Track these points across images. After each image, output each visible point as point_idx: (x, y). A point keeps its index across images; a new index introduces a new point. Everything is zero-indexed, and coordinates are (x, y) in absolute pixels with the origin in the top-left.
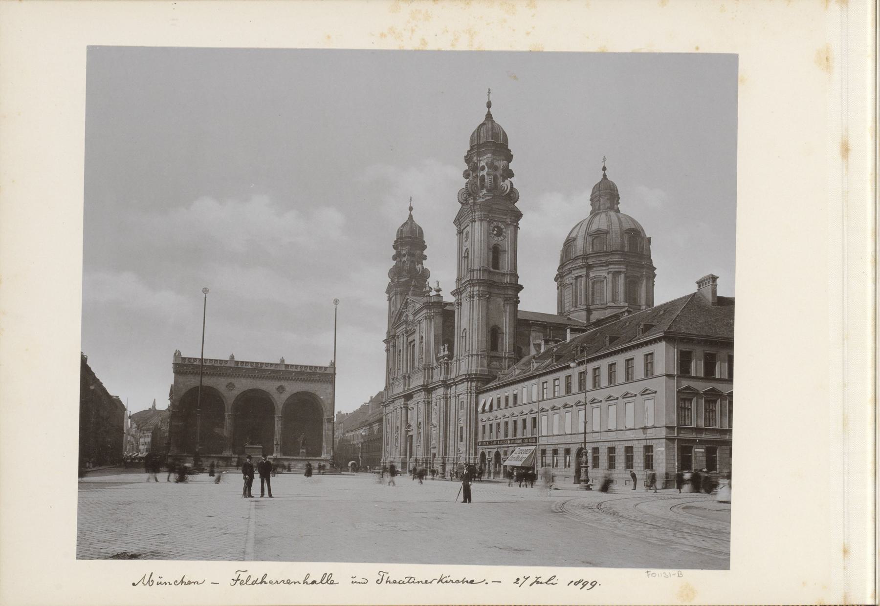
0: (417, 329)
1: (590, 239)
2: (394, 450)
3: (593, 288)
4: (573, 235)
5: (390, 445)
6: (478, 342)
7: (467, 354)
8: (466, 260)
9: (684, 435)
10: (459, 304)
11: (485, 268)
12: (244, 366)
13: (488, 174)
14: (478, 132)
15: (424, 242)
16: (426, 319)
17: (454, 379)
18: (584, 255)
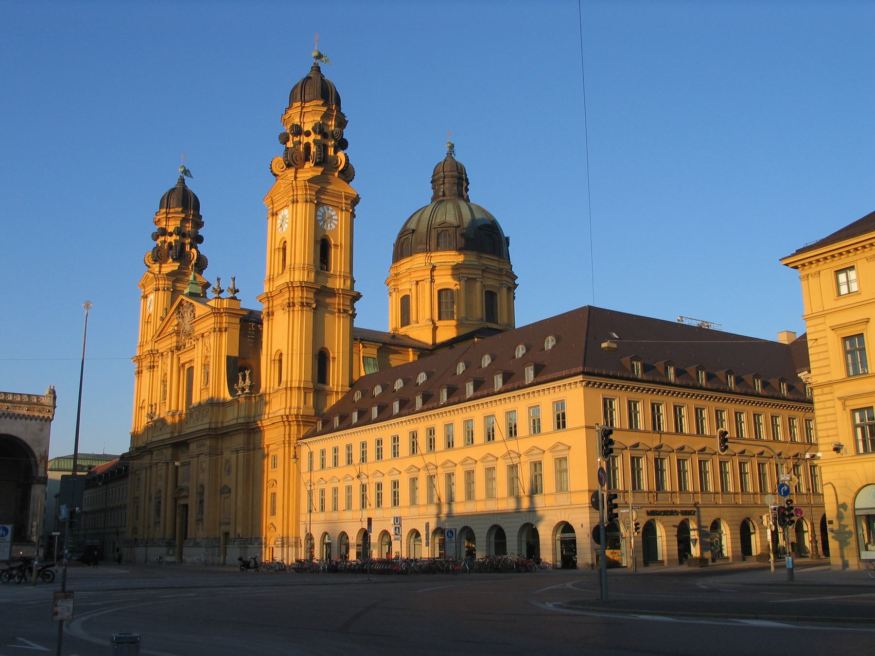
4: (412, 226)
10: (270, 314)
13: (315, 141)
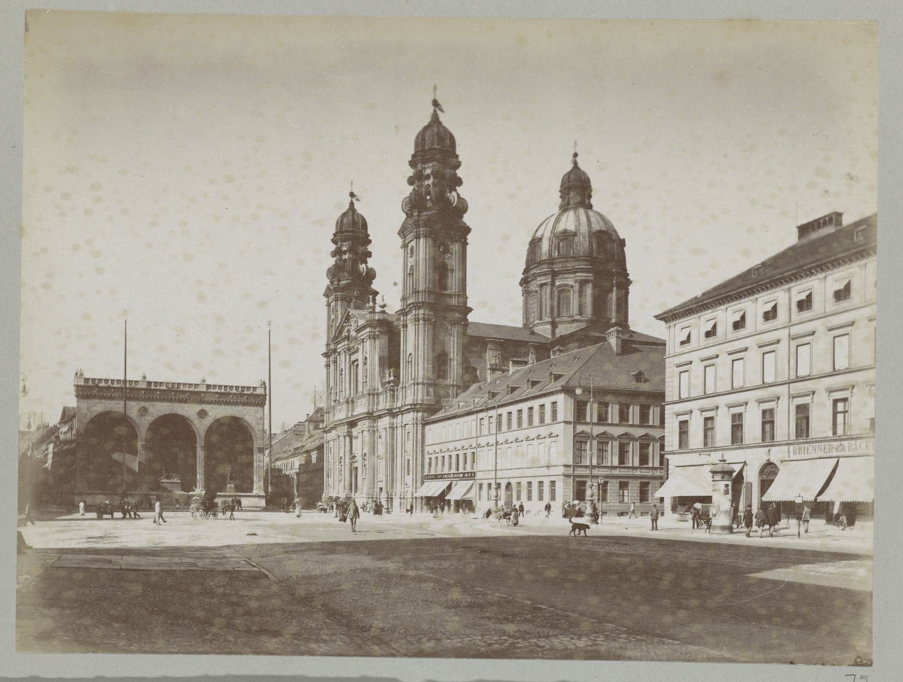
0: (361, 347)
1: (555, 242)
2: (337, 483)
3: (559, 298)
4: (539, 235)
5: (332, 478)
6: (424, 370)
7: (412, 382)
8: (411, 277)
9: (579, 472)
11: (430, 290)
12: (158, 387)
14: (422, 135)
15: (368, 235)
16: (370, 339)
17: (399, 408)
18: (550, 260)
